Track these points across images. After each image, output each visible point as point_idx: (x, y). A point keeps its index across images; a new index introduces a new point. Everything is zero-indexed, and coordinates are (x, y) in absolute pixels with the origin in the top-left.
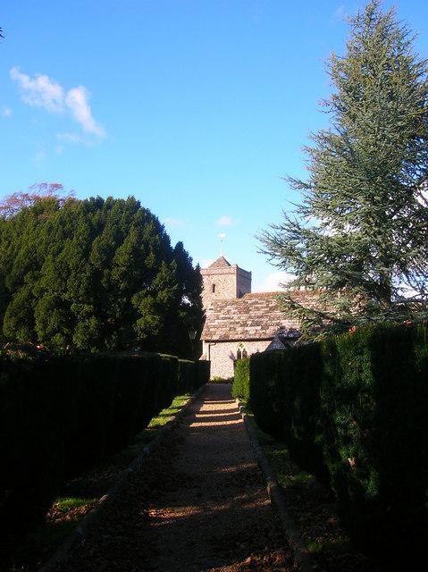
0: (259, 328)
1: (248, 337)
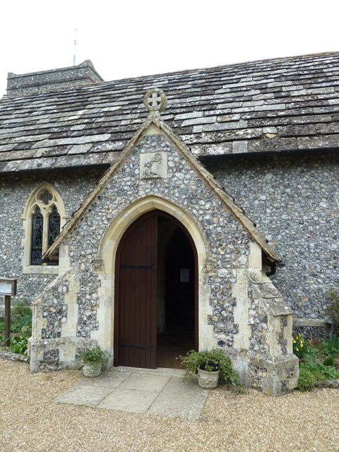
0: (107, 137)
1: (62, 162)
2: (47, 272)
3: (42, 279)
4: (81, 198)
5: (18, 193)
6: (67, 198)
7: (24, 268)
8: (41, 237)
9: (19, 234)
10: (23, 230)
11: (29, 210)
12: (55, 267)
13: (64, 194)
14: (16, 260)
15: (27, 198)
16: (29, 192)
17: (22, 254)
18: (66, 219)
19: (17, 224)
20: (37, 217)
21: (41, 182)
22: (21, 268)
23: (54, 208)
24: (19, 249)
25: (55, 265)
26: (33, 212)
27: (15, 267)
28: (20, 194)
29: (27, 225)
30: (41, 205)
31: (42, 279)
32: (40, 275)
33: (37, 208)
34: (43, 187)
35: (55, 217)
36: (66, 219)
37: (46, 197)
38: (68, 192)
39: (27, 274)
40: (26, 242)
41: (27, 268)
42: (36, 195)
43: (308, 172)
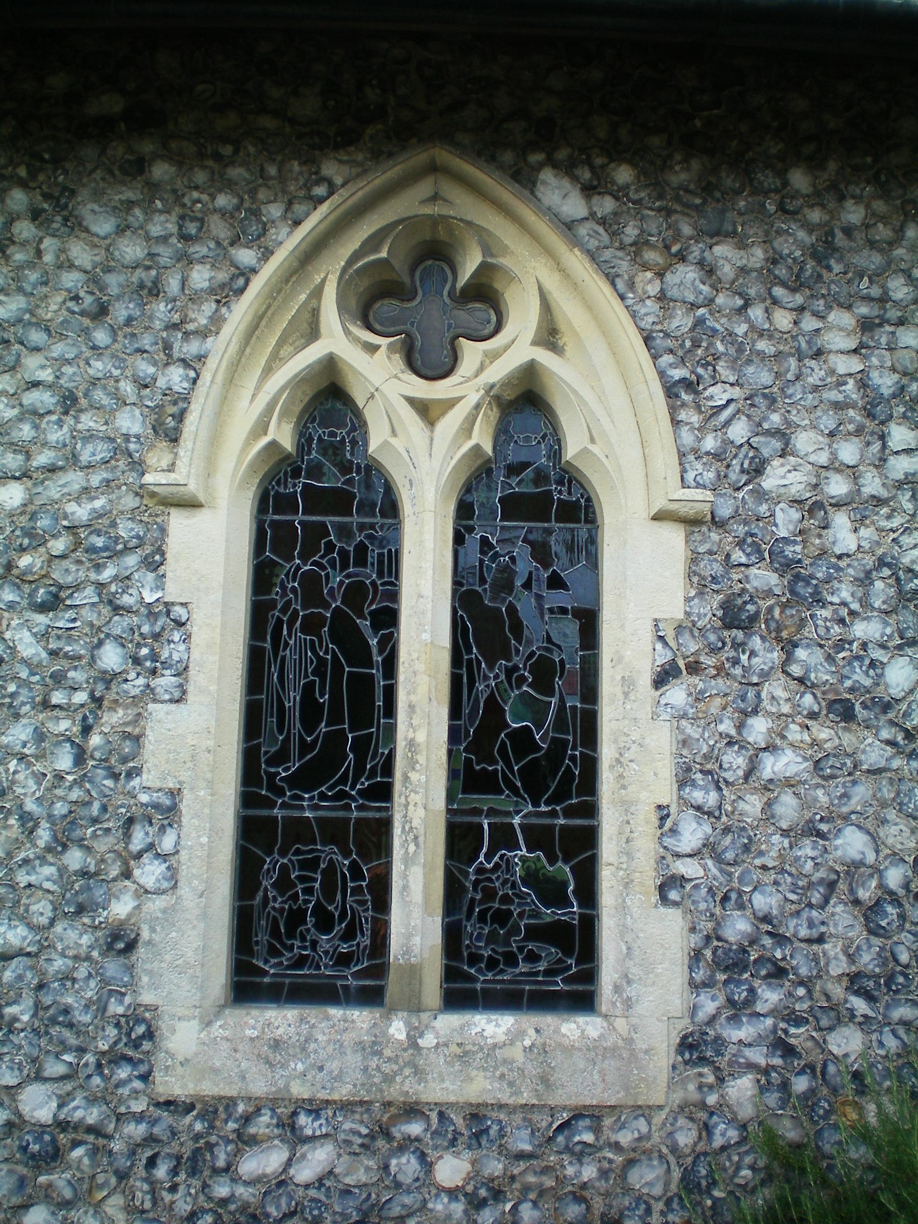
2: (480, 1087)
3: (406, 1166)
4: (837, 340)
5: (110, 237)
6: (681, 321)
7: (182, 1038)
8: (361, 695)
9: (111, 657)
10: (169, 619)
11: (246, 410)
12: (573, 1028)
13: (649, 284)
14: (76, 937)
15: (227, 293)
16: (251, 229)
17: (150, 873)
18: (691, 523)
19: (94, 544)
20: (319, 515)
21: (378, 155)
22: (139, 1036)
23: (525, 402)
24: (113, 816)
25: (543, 1001)
26: (284, 435)
27: (52, 1018)
28: (131, 250)
29: (209, 564)
30: (379, 376)
31: (406, 1166)
32: (384, 1124)
33: (329, 401)
34: (408, 204)
35: (531, 504)
36: (691, 523)
37: (424, 297)
38: (685, 278)
39: (212, 1110)
40: (194, 740)
41: (208, 1041)
42: (329, 274)
43: (816, 199)
